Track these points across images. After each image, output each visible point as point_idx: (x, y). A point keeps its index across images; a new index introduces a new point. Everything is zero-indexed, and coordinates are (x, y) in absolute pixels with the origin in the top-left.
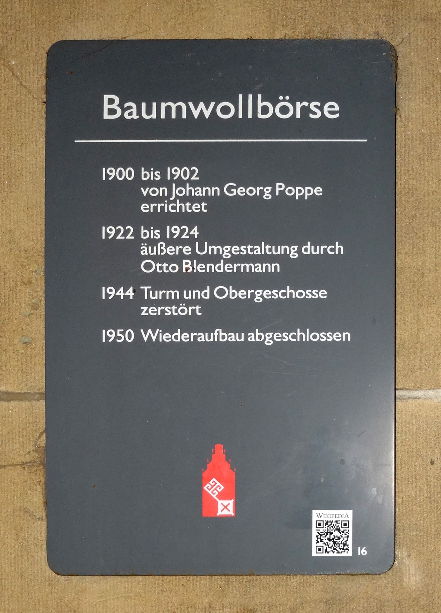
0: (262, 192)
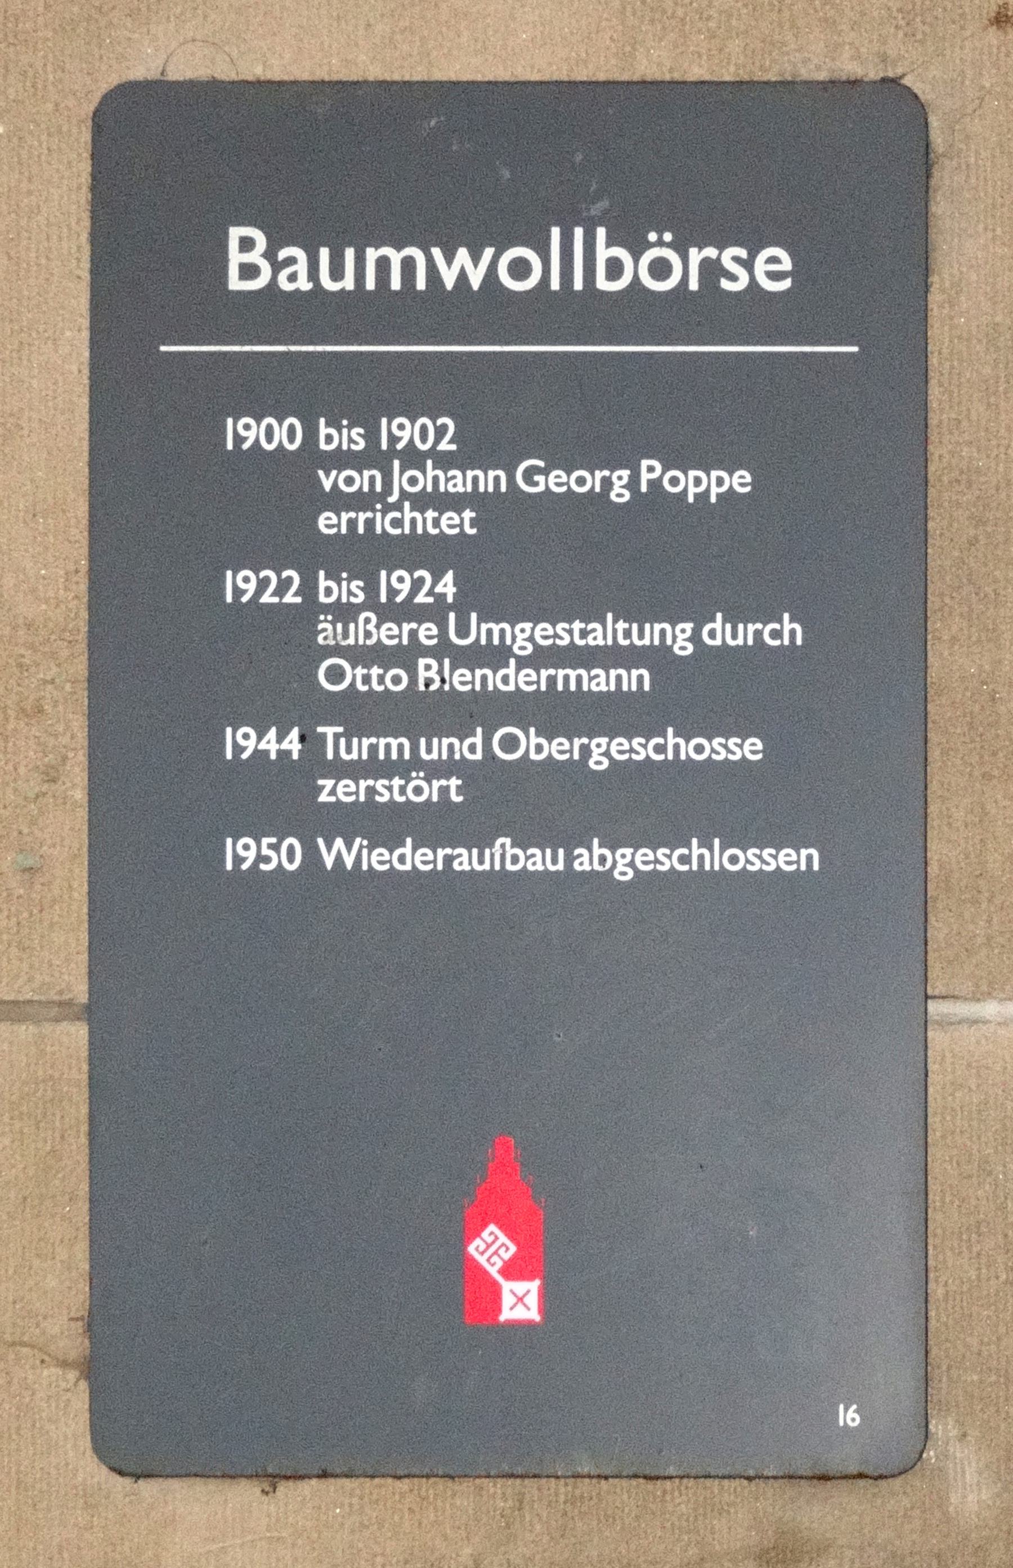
0: (607, 483)
